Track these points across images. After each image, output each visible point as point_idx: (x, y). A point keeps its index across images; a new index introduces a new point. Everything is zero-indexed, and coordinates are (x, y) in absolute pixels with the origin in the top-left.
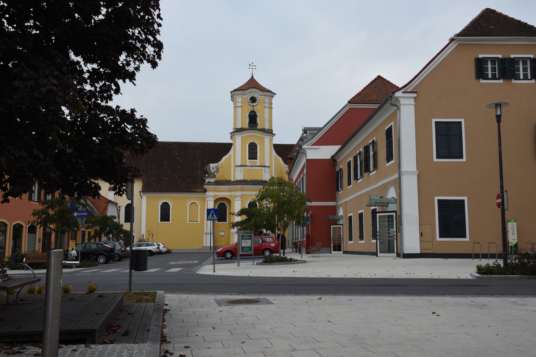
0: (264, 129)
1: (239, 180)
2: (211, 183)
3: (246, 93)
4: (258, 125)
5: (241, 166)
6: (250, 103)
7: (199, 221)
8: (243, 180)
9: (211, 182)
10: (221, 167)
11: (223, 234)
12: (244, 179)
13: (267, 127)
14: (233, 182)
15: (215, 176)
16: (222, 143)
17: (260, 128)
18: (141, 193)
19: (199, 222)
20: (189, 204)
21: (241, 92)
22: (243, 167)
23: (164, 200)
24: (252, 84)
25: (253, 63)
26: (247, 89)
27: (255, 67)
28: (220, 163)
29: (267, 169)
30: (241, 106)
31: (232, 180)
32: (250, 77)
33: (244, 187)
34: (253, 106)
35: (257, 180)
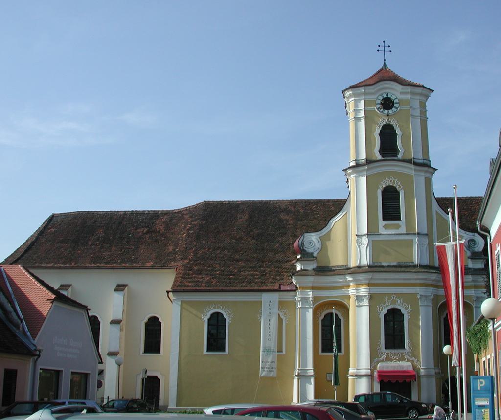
13: (419, 157)
18: (170, 294)
23: (215, 308)
24: (385, 76)
25: (384, 42)
27: (389, 49)
32: (381, 66)
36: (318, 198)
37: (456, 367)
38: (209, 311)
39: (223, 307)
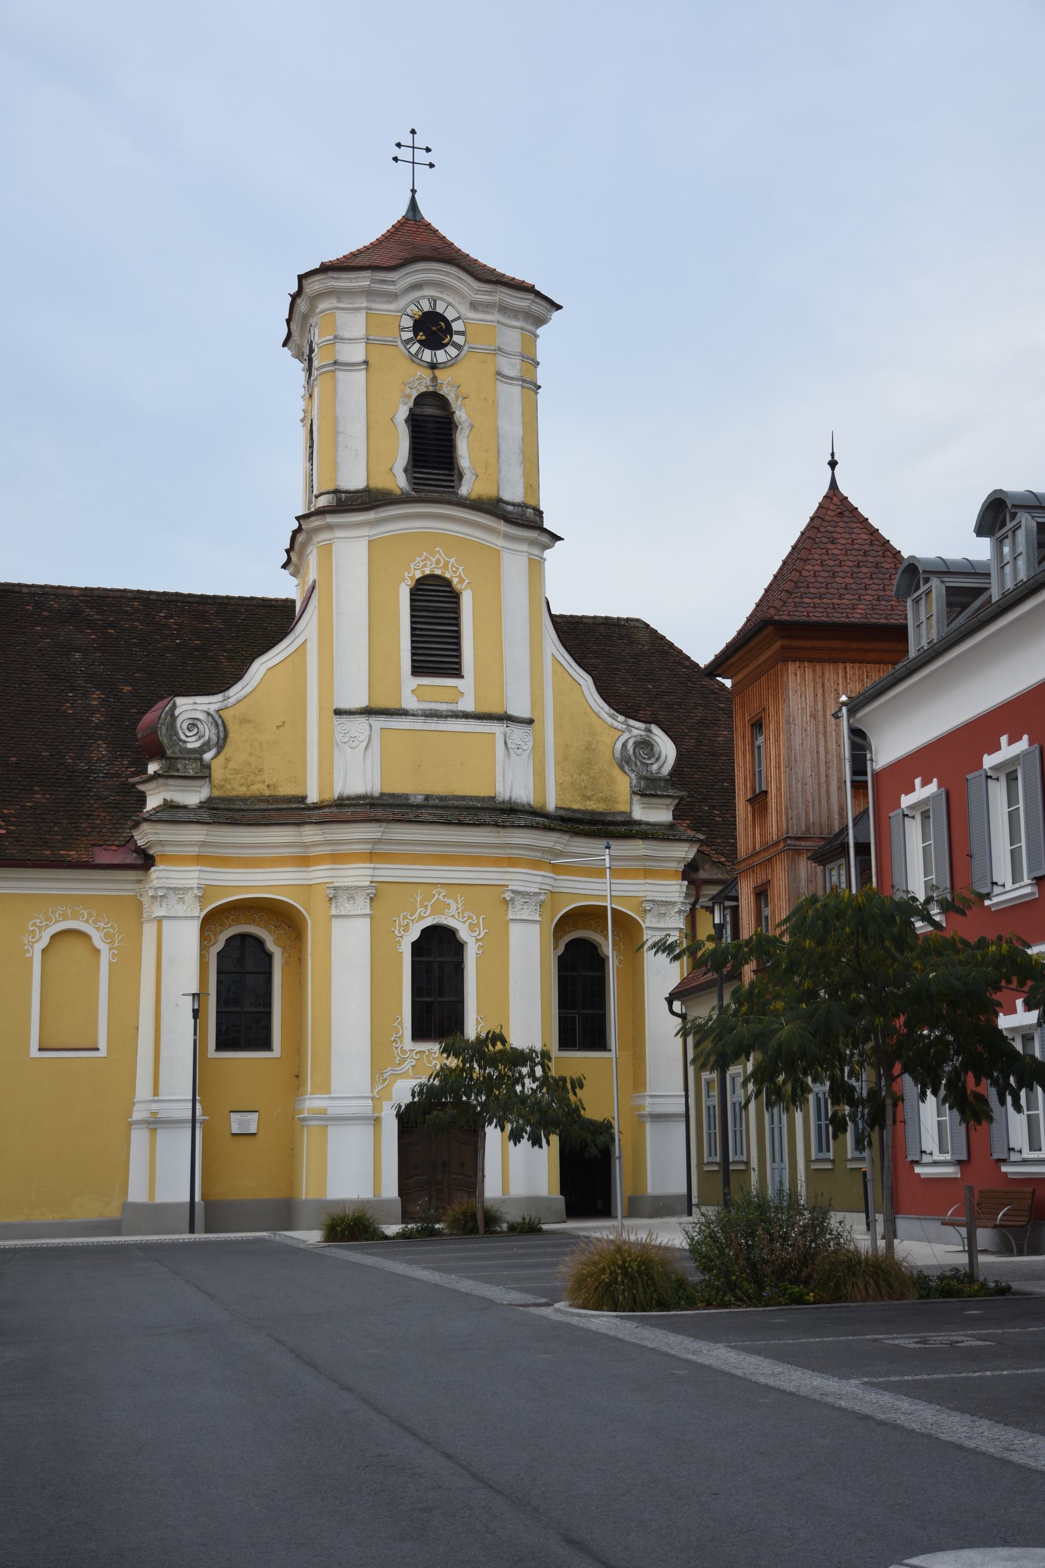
0: (500, 500)
1: (359, 797)
2: (180, 815)
3: (391, 288)
4: (461, 476)
5: (368, 712)
6: (417, 346)
7: (102, 1044)
8: (382, 794)
9: (185, 807)
10: (244, 720)
11: (251, 1123)
12: (389, 790)
13: (513, 493)
14: (316, 807)
15: (204, 773)
16: (215, 597)
17: (473, 496)
19: (103, 1052)
20: (45, 942)
21: (362, 280)
22: (382, 718)
23: (65, 918)
25: (413, 132)
26: (394, 263)
27: (427, 158)
28: (236, 692)
29: (517, 733)
30: (366, 362)
31: (313, 797)
32: (399, 211)
33: (387, 836)
34: (433, 366)
35: (463, 798)
36: (172, 589)
37: (803, 1077)
38: (47, 926)
39: (90, 915)
